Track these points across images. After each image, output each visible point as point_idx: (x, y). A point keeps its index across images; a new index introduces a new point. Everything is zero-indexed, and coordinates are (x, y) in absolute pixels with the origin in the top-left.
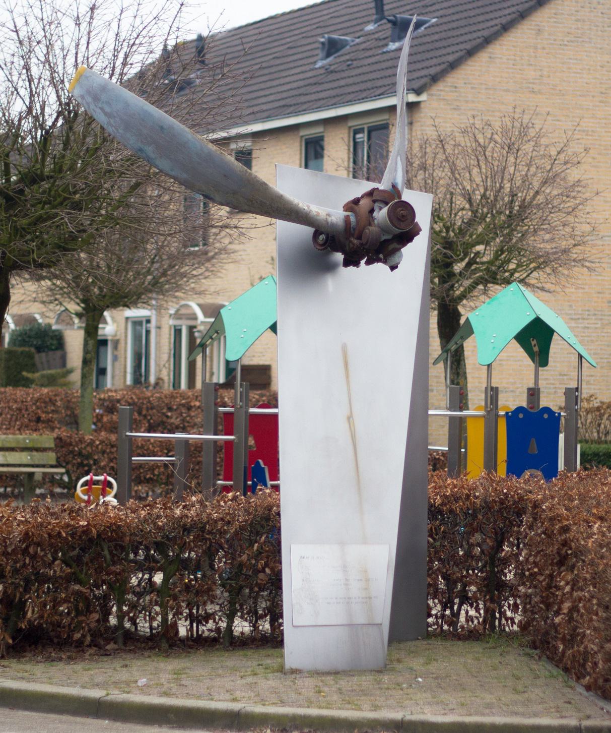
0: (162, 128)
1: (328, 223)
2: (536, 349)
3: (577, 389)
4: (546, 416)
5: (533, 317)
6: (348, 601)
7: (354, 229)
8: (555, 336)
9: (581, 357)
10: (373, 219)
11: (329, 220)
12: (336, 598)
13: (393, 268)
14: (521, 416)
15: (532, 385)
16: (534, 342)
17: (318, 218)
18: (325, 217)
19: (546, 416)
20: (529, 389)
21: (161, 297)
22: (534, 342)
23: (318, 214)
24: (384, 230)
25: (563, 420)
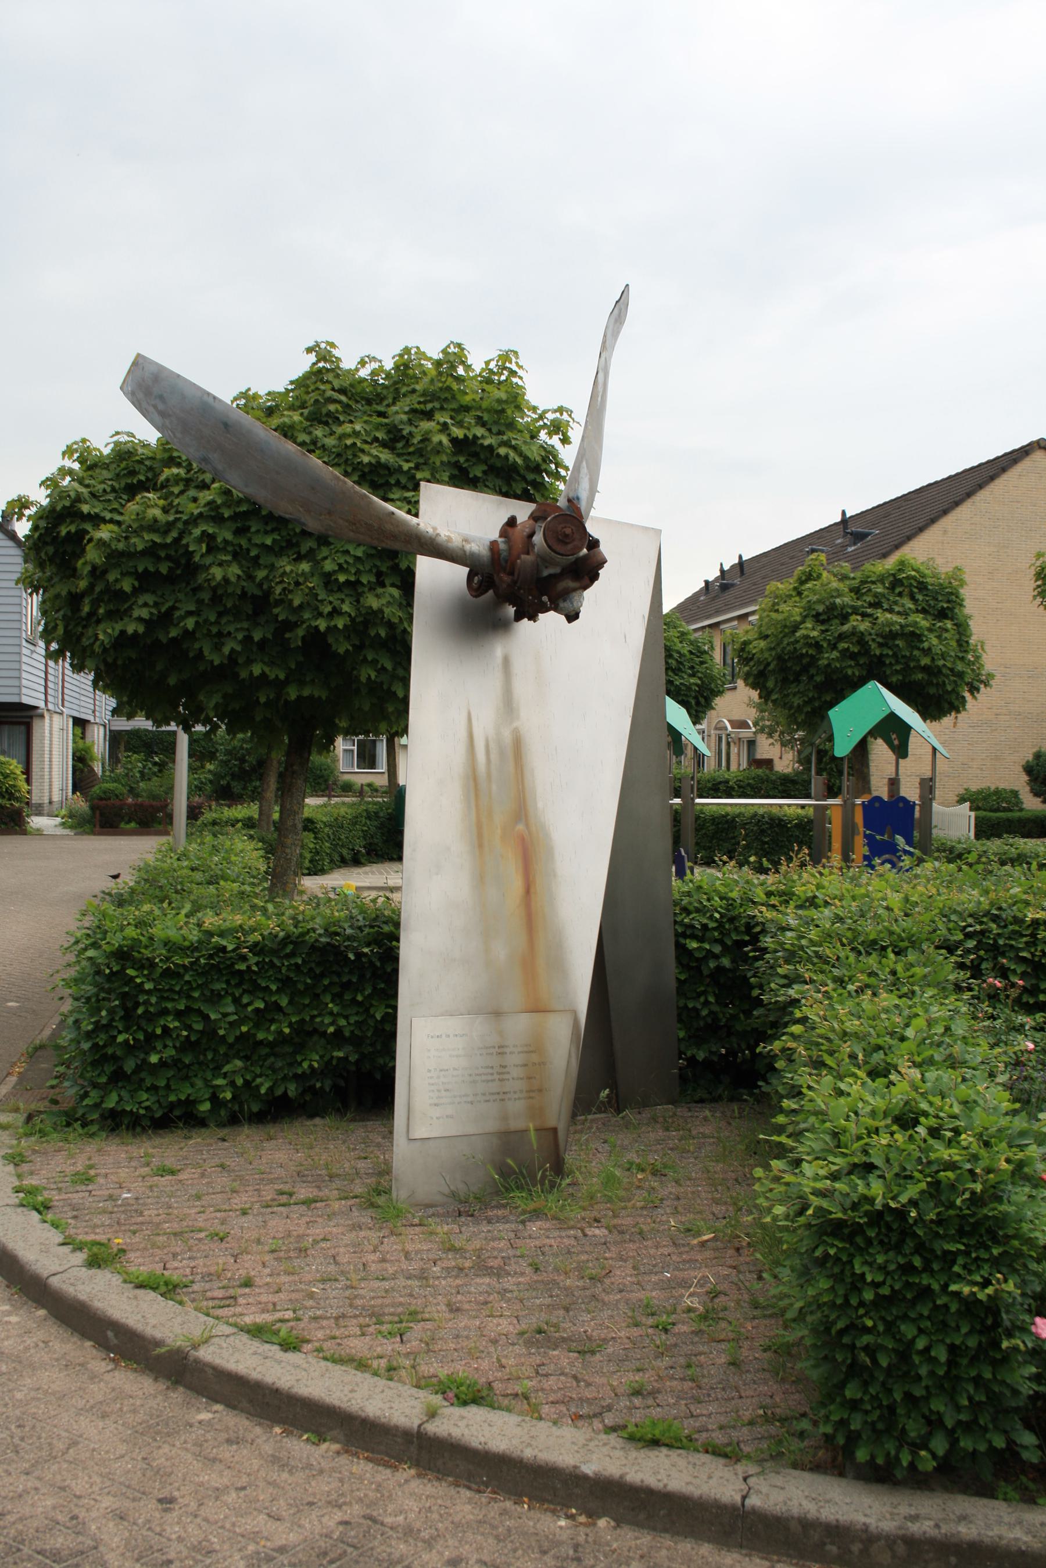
0: (226, 425)
1: (465, 551)
2: (896, 742)
3: (931, 780)
4: (901, 805)
5: (888, 712)
6: (502, 1096)
7: (506, 562)
8: (912, 732)
9: (934, 749)
10: (533, 546)
11: (467, 547)
12: (484, 1094)
13: (572, 617)
14: (901, 805)
15: (893, 776)
16: (894, 736)
17: (450, 545)
18: (460, 545)
19: (877, 805)
20: (890, 779)
21: (41, 628)
22: (894, 736)
23: (449, 539)
24: (543, 560)
25: (917, 808)
